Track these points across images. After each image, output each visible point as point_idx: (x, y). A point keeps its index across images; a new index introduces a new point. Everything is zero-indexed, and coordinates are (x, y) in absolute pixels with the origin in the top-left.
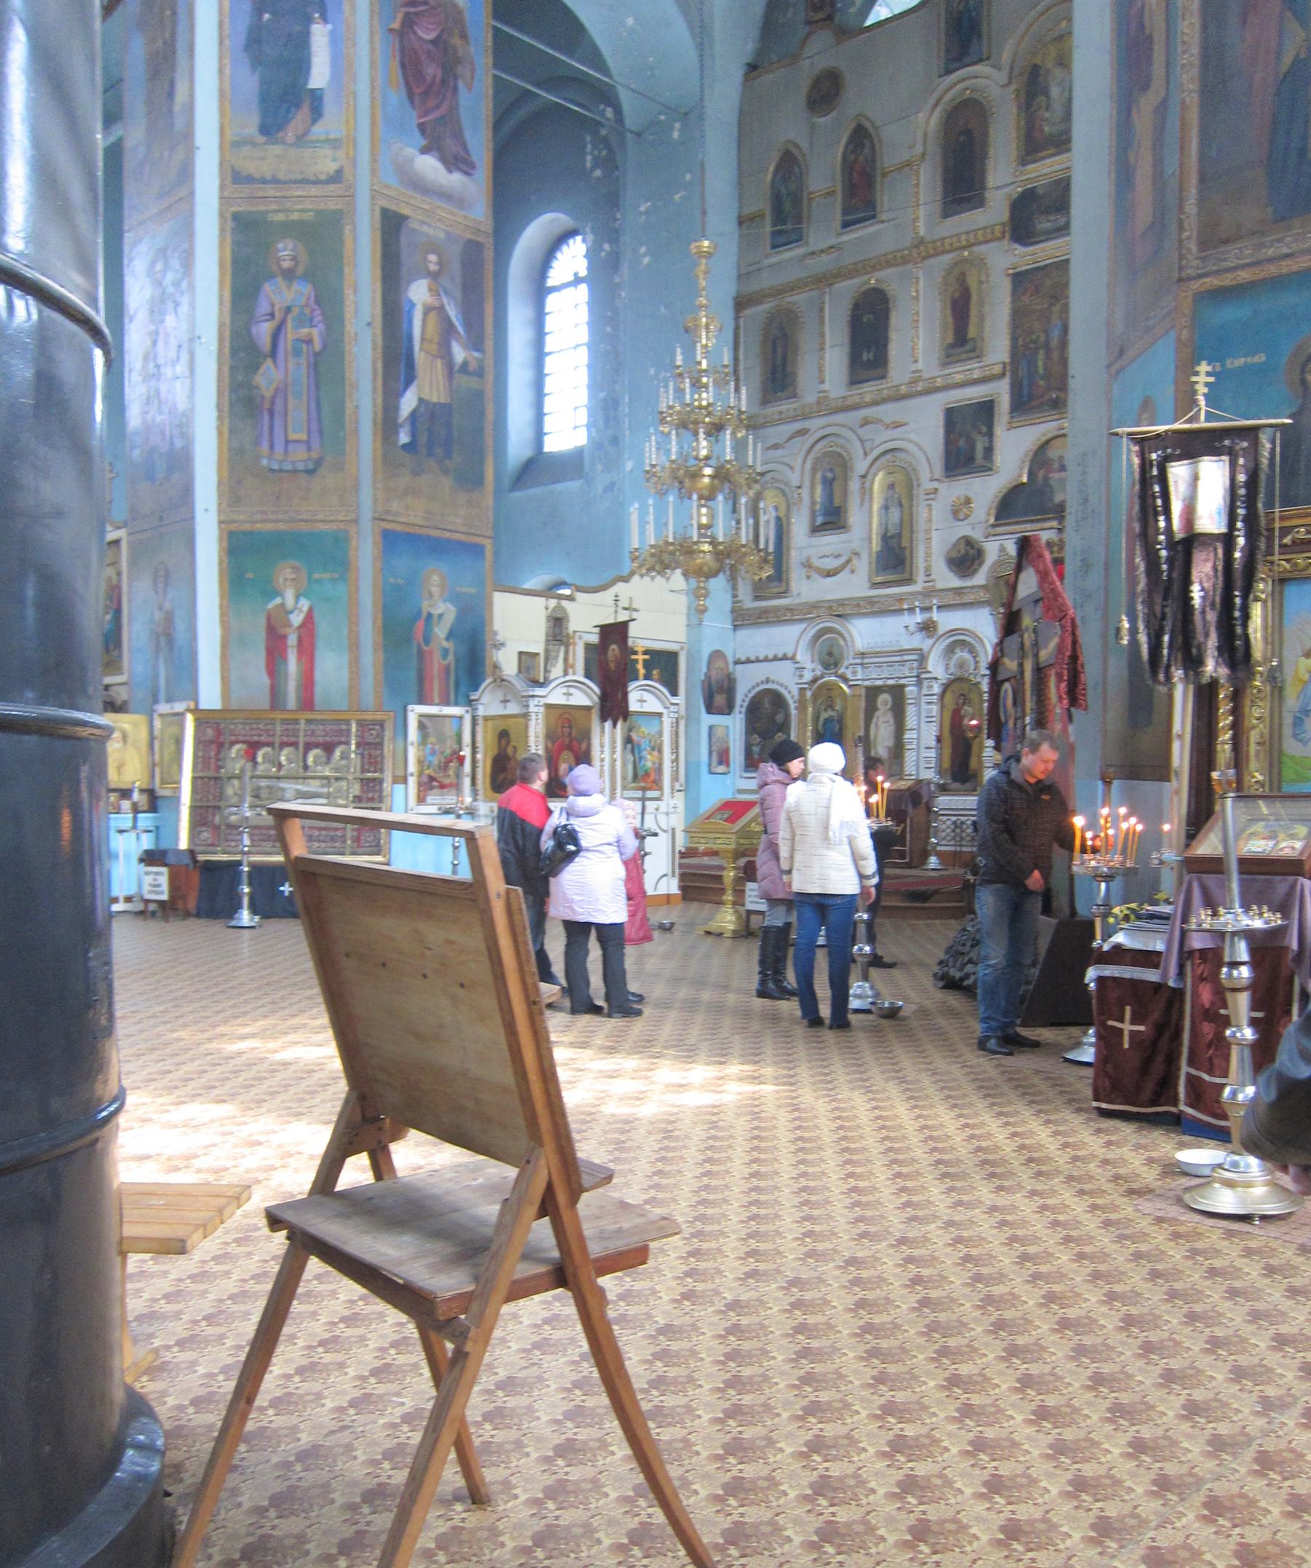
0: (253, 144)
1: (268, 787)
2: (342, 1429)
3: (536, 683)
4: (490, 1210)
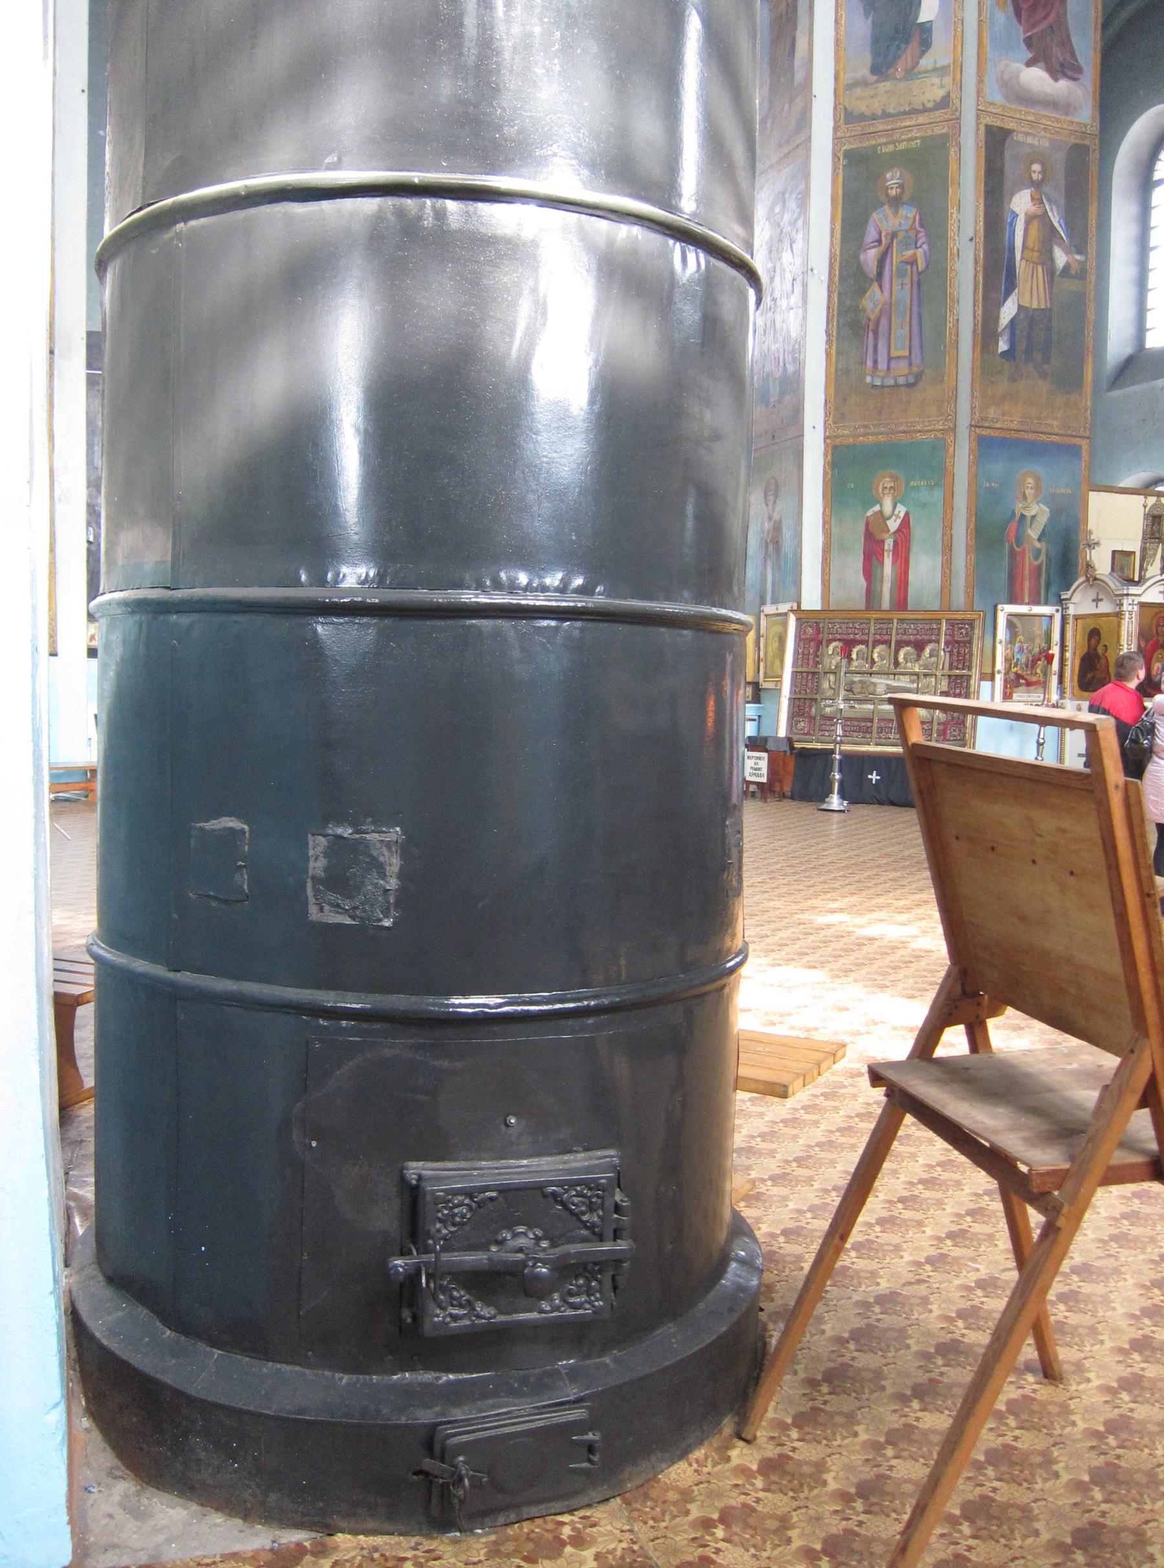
0: (864, 83)
1: (860, 681)
2: (919, 1282)
3: (1131, 582)
4: (1089, 1096)
